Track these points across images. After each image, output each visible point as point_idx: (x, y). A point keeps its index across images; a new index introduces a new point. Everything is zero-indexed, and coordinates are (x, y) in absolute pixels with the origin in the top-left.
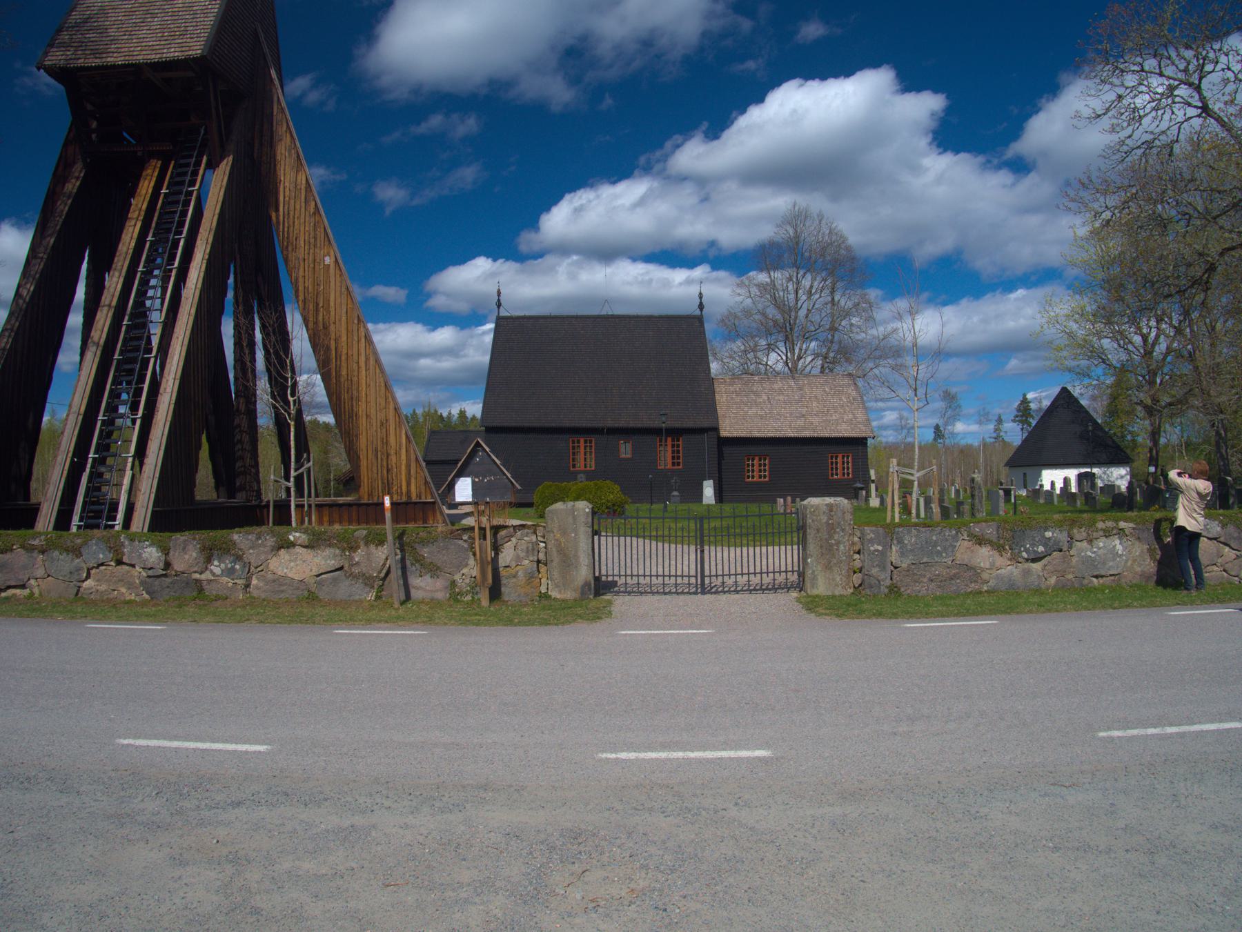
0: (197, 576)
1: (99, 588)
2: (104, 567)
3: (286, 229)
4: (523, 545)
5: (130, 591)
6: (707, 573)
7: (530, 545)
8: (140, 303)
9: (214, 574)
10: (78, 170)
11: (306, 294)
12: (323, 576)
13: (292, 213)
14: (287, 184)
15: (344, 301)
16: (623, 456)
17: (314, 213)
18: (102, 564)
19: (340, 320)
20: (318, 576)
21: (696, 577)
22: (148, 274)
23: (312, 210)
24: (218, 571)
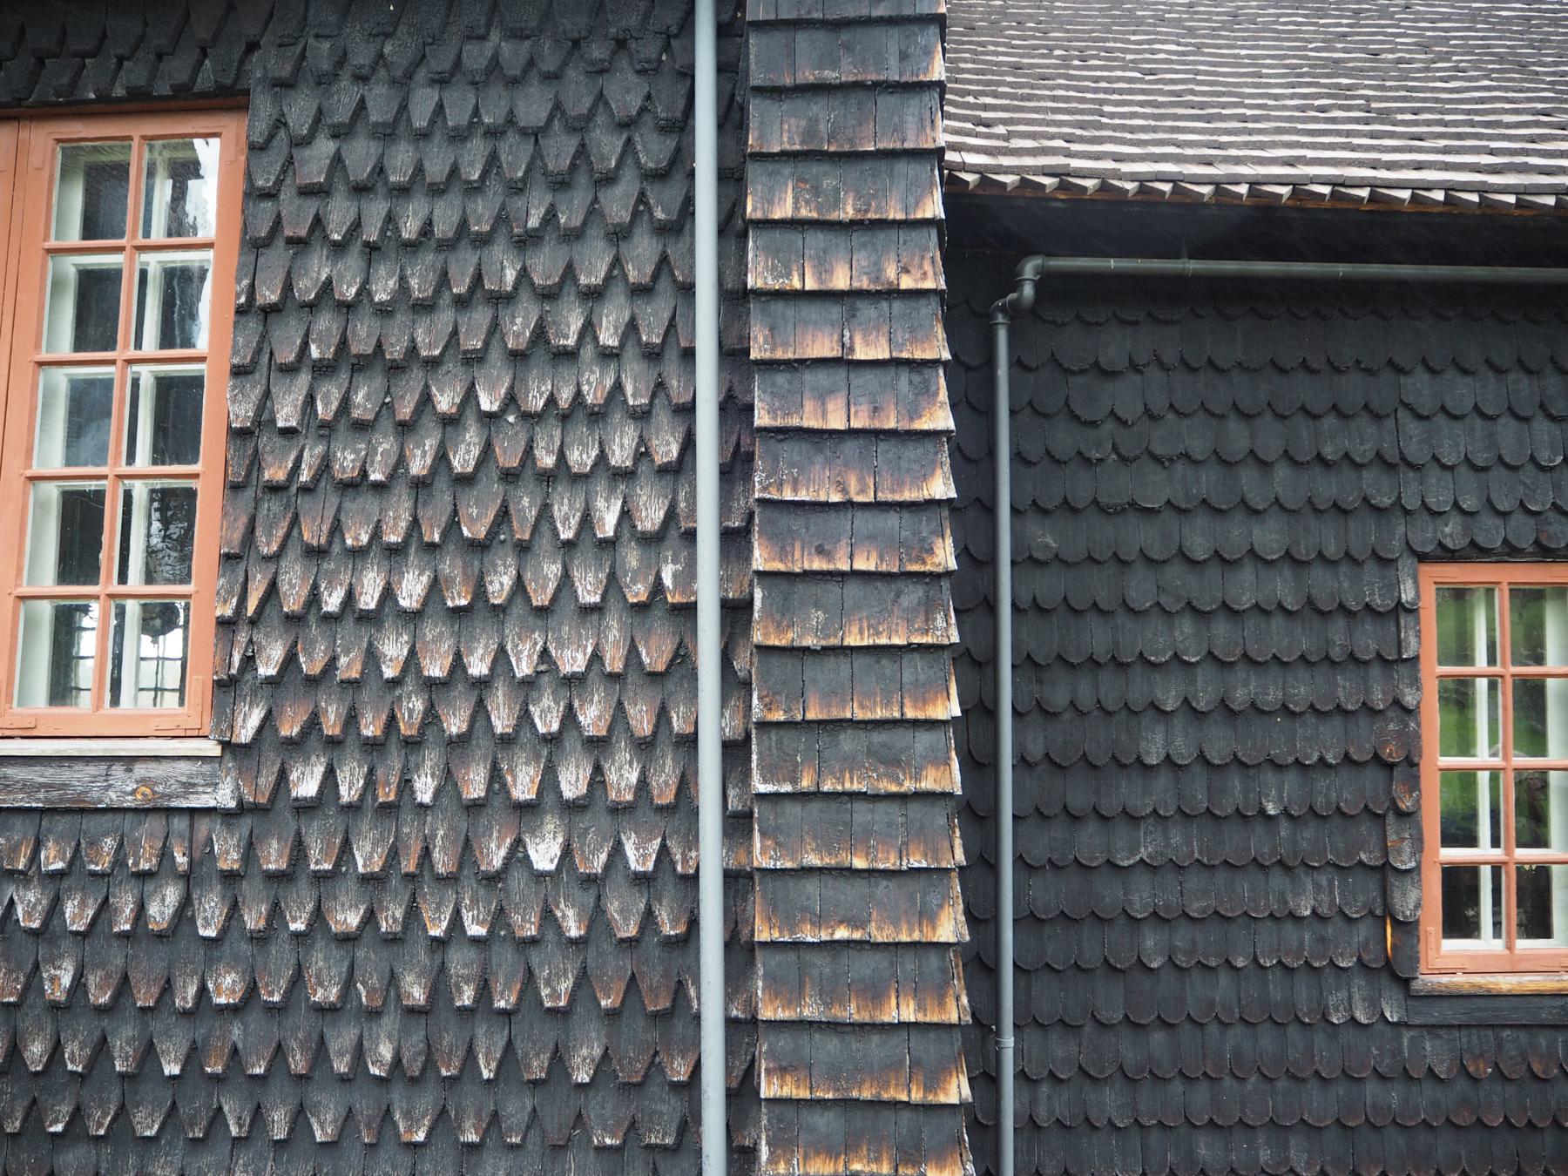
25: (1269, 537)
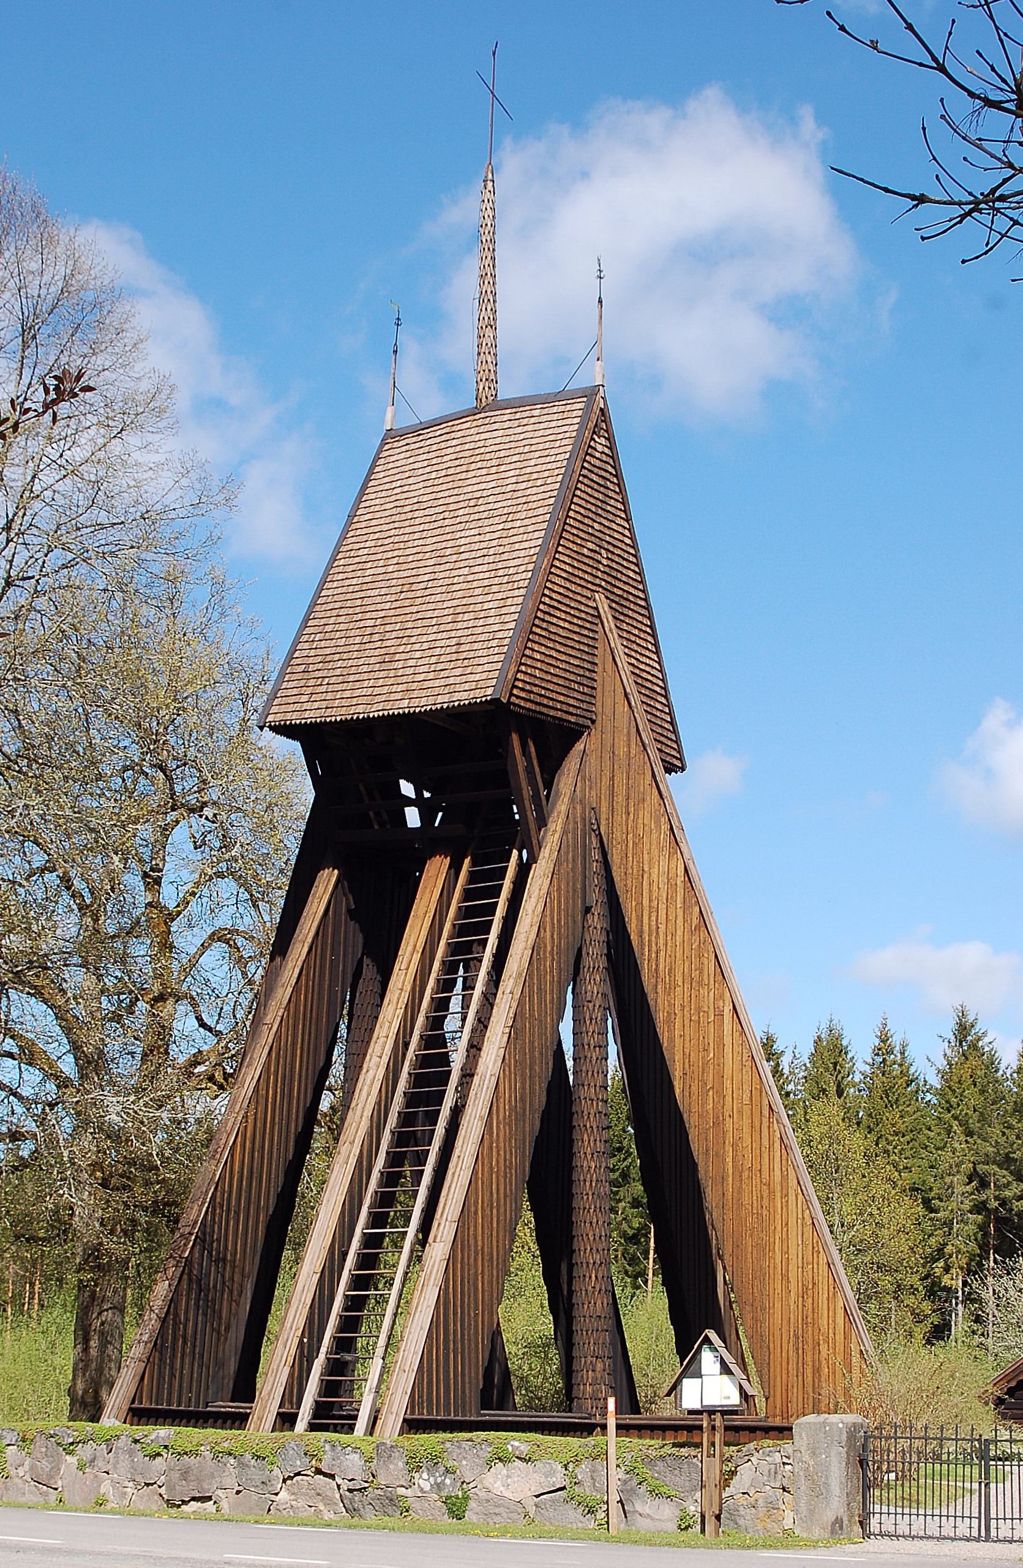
0: (401, 1491)
1: (293, 1503)
2: (301, 1477)
3: (654, 955)
4: (764, 1467)
5: (328, 1508)
6: (993, 1515)
7: (773, 1467)
8: (436, 1023)
9: (422, 1490)
10: (327, 880)
11: (687, 1066)
12: (542, 1497)
13: (662, 927)
14: (655, 877)
15: (747, 1078)
17: (698, 927)
18: (298, 1474)
19: (740, 1112)
20: (537, 1496)
21: (979, 1518)
22: (447, 986)
23: (695, 922)
24: (427, 1486)
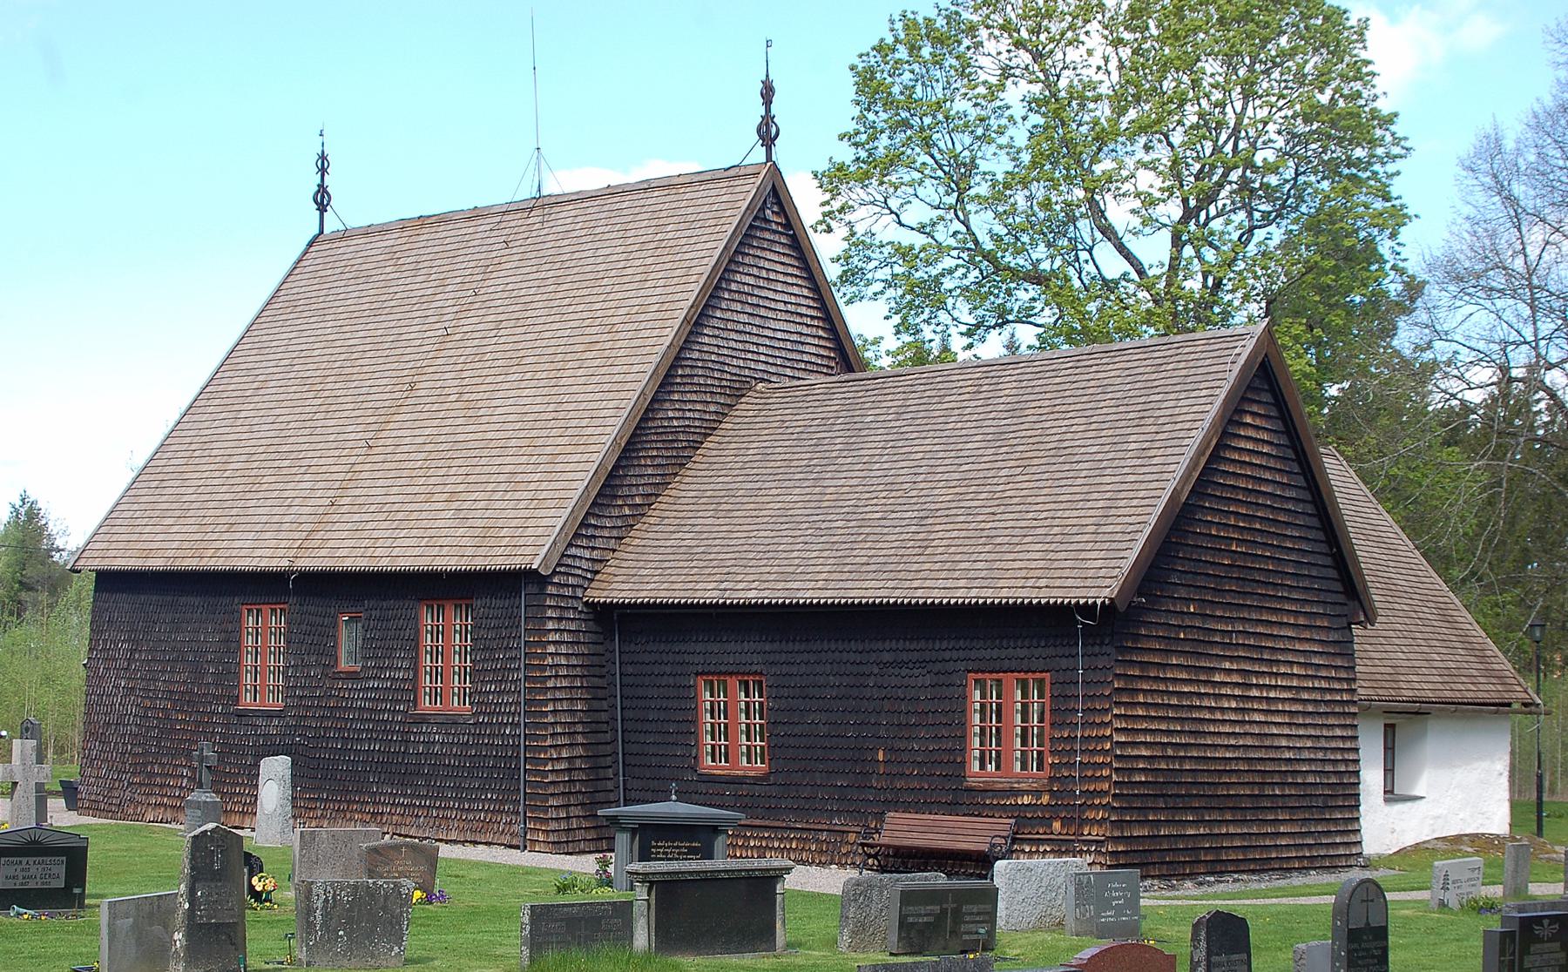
16: (344, 664)
25: (668, 669)
